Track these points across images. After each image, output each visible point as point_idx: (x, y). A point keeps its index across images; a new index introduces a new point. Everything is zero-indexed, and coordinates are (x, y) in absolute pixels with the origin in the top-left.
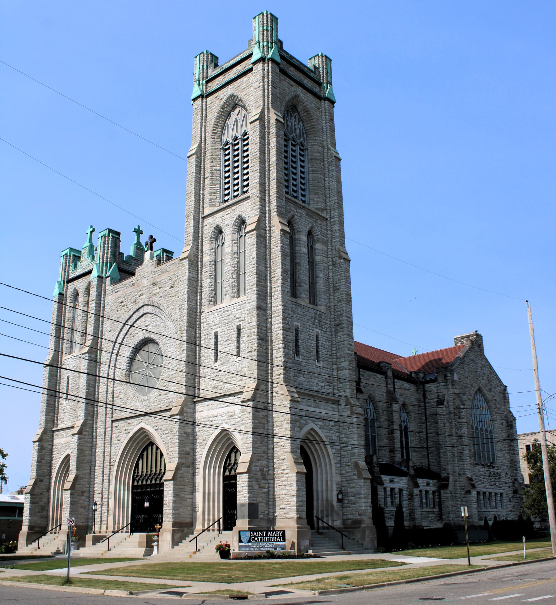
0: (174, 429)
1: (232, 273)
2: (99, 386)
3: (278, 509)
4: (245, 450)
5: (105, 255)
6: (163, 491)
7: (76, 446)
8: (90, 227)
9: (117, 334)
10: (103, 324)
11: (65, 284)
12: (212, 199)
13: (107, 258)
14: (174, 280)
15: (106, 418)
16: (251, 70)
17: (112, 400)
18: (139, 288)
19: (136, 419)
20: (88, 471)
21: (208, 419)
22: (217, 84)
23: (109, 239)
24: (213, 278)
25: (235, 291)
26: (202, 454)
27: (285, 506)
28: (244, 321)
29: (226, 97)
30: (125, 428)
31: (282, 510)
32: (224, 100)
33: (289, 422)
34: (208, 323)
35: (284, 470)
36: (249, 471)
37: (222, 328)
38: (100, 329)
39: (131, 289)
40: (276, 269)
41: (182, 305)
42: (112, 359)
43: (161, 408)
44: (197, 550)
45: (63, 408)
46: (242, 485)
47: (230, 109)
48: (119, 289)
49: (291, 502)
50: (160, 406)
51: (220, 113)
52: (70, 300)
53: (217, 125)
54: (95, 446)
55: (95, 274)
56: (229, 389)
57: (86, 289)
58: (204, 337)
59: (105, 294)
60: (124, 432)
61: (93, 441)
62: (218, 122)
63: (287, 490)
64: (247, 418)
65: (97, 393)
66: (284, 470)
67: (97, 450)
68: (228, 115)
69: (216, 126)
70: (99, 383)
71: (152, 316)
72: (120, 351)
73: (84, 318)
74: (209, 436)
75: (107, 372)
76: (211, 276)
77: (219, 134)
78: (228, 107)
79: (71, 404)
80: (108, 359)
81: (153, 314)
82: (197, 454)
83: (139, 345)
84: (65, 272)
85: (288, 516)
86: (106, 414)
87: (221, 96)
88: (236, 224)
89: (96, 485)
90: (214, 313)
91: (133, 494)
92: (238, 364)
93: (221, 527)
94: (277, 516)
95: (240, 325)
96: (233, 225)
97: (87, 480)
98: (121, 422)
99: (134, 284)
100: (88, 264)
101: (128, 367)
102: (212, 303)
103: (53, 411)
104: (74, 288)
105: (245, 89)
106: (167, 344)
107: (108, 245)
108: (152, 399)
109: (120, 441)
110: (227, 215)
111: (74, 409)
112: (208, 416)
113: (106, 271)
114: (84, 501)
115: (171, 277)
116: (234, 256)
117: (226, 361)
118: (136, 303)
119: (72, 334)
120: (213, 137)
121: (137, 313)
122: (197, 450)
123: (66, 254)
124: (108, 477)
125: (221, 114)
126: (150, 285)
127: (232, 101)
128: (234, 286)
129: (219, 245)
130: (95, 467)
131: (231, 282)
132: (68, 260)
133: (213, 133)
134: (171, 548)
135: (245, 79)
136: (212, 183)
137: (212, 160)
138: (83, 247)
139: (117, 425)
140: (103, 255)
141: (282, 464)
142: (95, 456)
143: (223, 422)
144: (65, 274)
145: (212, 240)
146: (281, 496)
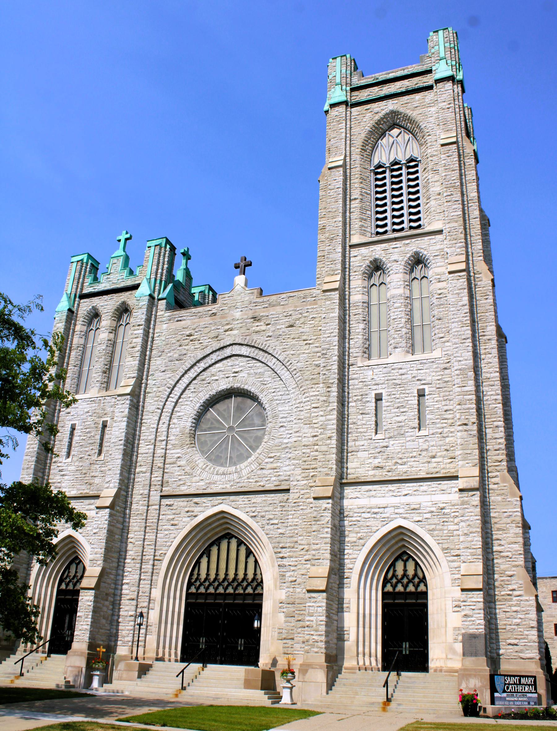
0: (322, 518)
1: (406, 322)
2: (138, 444)
3: (503, 645)
4: (469, 557)
5: (160, 271)
6: (77, 601)
7: (106, 526)
8: (125, 232)
9: (178, 377)
10: (150, 360)
11: (77, 299)
12: (362, 226)
13: (162, 275)
14: (294, 317)
15: (150, 490)
16: (430, 88)
17: (162, 466)
18: (225, 320)
19: (211, 498)
20: (115, 565)
21: (368, 510)
22: (369, 95)
23: (165, 251)
24: (366, 324)
25: (409, 345)
26: (355, 559)
27: (517, 641)
28: (430, 386)
29: (384, 112)
30: (187, 509)
31: (511, 647)
32: (381, 115)
33: (520, 525)
34: (364, 380)
35: (514, 590)
36: (97, 588)
37: (390, 390)
38: (146, 366)
39: (208, 320)
40: (487, 326)
41: (329, 349)
42: (164, 410)
43: (263, 486)
44: (183, 688)
45: (61, 468)
46: (473, 607)
47: (386, 128)
48: (184, 318)
49: (527, 635)
50: (262, 484)
51: (374, 129)
52: (83, 321)
53: (367, 141)
54: (127, 528)
55: (144, 290)
56: (406, 473)
57: (115, 310)
58: (355, 398)
59: (155, 321)
60: (183, 514)
61: (124, 521)
62: (369, 139)
63: (520, 618)
64: (471, 514)
65: (135, 454)
66: (514, 590)
67: (129, 536)
68: (382, 135)
69: (366, 142)
70: (139, 440)
71: (248, 361)
72: (180, 400)
73: (108, 348)
74: (371, 534)
75: (155, 426)
76: (364, 320)
77: (369, 152)
78: (384, 125)
79: (76, 464)
80: (158, 408)
81: (250, 357)
82: (346, 557)
83: (217, 397)
84: (78, 283)
85: (522, 655)
86: (150, 485)
87: (376, 110)
88: (410, 262)
89: (124, 587)
90: (374, 368)
91: (187, 605)
92: (421, 440)
93: (179, 658)
94: (502, 654)
95: (75, 424)
96: (406, 262)
97: (112, 577)
98: (179, 500)
99: (214, 314)
100: (123, 279)
101: (194, 425)
102: (366, 355)
103: (42, 471)
104: (93, 307)
105: (418, 108)
106: (276, 400)
107: (164, 259)
108: (244, 472)
109: (177, 527)
110: (394, 248)
111: (84, 471)
112: (368, 506)
113: (160, 290)
114: (107, 607)
115: (290, 313)
116: (407, 301)
117: (398, 434)
118: (218, 338)
119: (80, 368)
120: (362, 154)
121: (218, 353)
122: (346, 552)
123: (82, 260)
124: (150, 577)
125: (374, 130)
126: (247, 319)
127: (391, 119)
128: (409, 338)
129: (92, 329)
130: (125, 559)
131: (404, 333)
132: (84, 268)
133: (362, 149)
134: (325, 694)
135: (417, 97)
136: (361, 208)
137: (361, 180)
138: (113, 256)
139: (172, 503)
140: (157, 269)
141: (509, 583)
142: (126, 543)
143: (398, 516)
144: (77, 286)
145: (365, 277)
146: (508, 627)
